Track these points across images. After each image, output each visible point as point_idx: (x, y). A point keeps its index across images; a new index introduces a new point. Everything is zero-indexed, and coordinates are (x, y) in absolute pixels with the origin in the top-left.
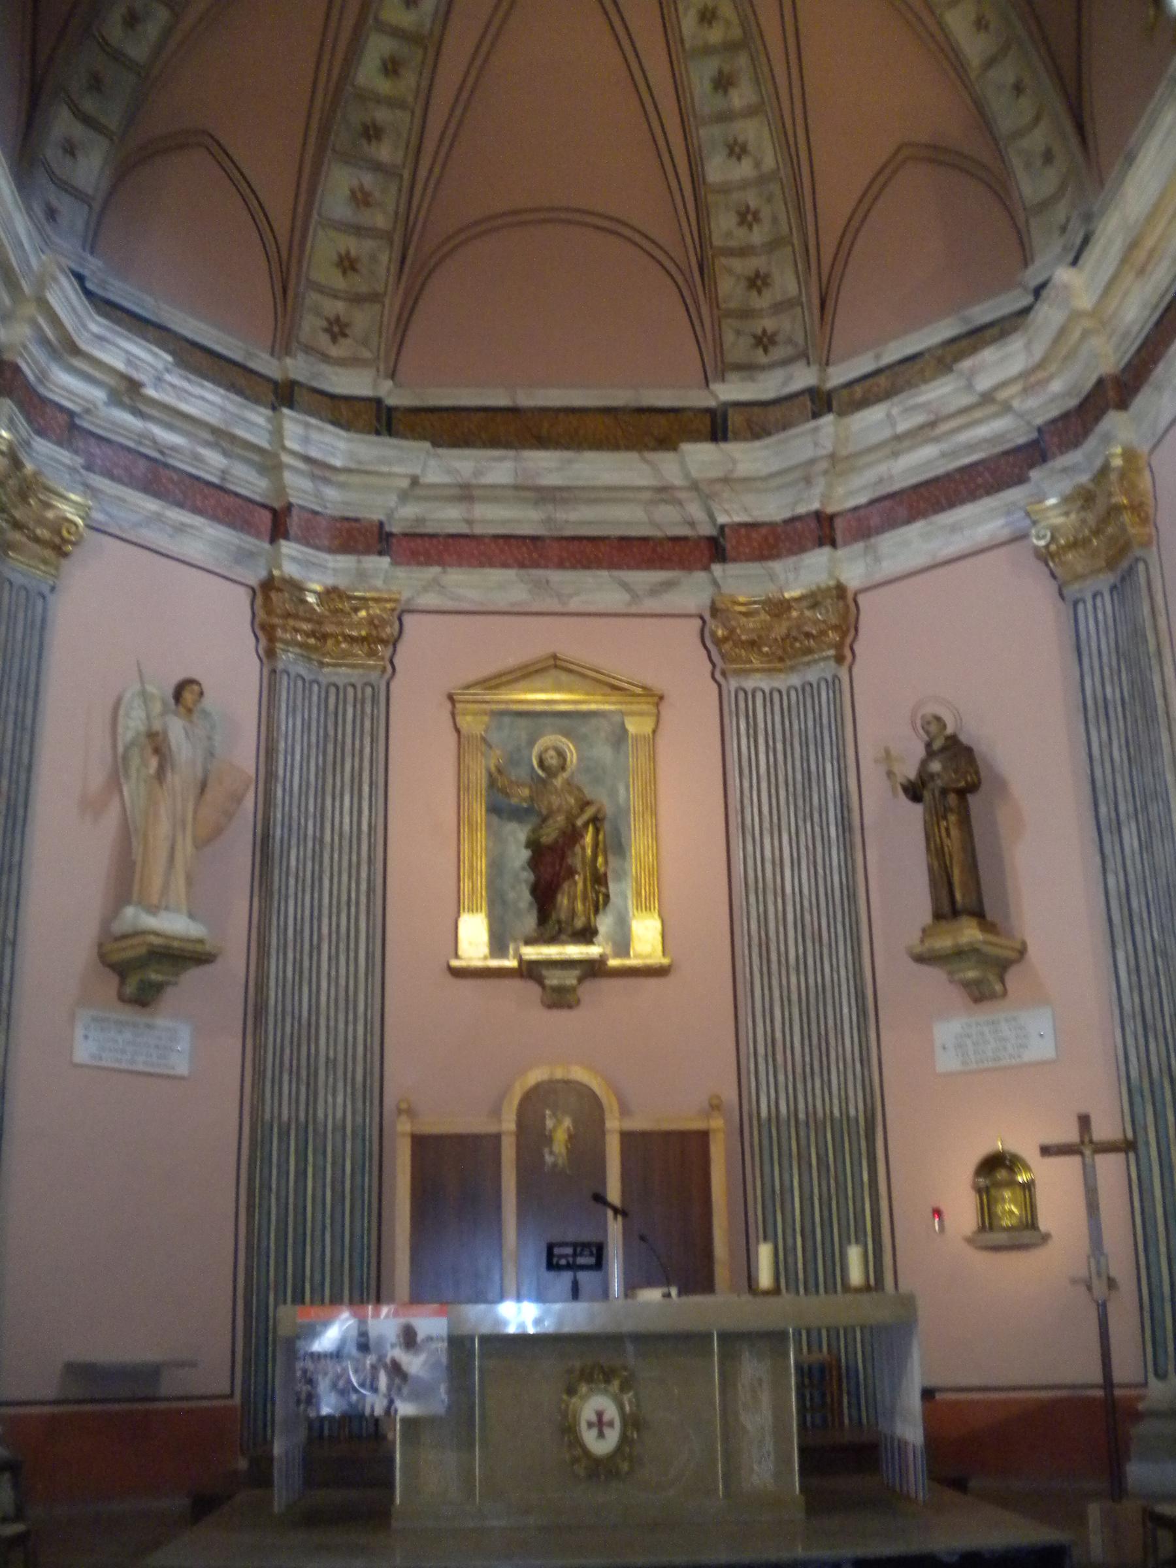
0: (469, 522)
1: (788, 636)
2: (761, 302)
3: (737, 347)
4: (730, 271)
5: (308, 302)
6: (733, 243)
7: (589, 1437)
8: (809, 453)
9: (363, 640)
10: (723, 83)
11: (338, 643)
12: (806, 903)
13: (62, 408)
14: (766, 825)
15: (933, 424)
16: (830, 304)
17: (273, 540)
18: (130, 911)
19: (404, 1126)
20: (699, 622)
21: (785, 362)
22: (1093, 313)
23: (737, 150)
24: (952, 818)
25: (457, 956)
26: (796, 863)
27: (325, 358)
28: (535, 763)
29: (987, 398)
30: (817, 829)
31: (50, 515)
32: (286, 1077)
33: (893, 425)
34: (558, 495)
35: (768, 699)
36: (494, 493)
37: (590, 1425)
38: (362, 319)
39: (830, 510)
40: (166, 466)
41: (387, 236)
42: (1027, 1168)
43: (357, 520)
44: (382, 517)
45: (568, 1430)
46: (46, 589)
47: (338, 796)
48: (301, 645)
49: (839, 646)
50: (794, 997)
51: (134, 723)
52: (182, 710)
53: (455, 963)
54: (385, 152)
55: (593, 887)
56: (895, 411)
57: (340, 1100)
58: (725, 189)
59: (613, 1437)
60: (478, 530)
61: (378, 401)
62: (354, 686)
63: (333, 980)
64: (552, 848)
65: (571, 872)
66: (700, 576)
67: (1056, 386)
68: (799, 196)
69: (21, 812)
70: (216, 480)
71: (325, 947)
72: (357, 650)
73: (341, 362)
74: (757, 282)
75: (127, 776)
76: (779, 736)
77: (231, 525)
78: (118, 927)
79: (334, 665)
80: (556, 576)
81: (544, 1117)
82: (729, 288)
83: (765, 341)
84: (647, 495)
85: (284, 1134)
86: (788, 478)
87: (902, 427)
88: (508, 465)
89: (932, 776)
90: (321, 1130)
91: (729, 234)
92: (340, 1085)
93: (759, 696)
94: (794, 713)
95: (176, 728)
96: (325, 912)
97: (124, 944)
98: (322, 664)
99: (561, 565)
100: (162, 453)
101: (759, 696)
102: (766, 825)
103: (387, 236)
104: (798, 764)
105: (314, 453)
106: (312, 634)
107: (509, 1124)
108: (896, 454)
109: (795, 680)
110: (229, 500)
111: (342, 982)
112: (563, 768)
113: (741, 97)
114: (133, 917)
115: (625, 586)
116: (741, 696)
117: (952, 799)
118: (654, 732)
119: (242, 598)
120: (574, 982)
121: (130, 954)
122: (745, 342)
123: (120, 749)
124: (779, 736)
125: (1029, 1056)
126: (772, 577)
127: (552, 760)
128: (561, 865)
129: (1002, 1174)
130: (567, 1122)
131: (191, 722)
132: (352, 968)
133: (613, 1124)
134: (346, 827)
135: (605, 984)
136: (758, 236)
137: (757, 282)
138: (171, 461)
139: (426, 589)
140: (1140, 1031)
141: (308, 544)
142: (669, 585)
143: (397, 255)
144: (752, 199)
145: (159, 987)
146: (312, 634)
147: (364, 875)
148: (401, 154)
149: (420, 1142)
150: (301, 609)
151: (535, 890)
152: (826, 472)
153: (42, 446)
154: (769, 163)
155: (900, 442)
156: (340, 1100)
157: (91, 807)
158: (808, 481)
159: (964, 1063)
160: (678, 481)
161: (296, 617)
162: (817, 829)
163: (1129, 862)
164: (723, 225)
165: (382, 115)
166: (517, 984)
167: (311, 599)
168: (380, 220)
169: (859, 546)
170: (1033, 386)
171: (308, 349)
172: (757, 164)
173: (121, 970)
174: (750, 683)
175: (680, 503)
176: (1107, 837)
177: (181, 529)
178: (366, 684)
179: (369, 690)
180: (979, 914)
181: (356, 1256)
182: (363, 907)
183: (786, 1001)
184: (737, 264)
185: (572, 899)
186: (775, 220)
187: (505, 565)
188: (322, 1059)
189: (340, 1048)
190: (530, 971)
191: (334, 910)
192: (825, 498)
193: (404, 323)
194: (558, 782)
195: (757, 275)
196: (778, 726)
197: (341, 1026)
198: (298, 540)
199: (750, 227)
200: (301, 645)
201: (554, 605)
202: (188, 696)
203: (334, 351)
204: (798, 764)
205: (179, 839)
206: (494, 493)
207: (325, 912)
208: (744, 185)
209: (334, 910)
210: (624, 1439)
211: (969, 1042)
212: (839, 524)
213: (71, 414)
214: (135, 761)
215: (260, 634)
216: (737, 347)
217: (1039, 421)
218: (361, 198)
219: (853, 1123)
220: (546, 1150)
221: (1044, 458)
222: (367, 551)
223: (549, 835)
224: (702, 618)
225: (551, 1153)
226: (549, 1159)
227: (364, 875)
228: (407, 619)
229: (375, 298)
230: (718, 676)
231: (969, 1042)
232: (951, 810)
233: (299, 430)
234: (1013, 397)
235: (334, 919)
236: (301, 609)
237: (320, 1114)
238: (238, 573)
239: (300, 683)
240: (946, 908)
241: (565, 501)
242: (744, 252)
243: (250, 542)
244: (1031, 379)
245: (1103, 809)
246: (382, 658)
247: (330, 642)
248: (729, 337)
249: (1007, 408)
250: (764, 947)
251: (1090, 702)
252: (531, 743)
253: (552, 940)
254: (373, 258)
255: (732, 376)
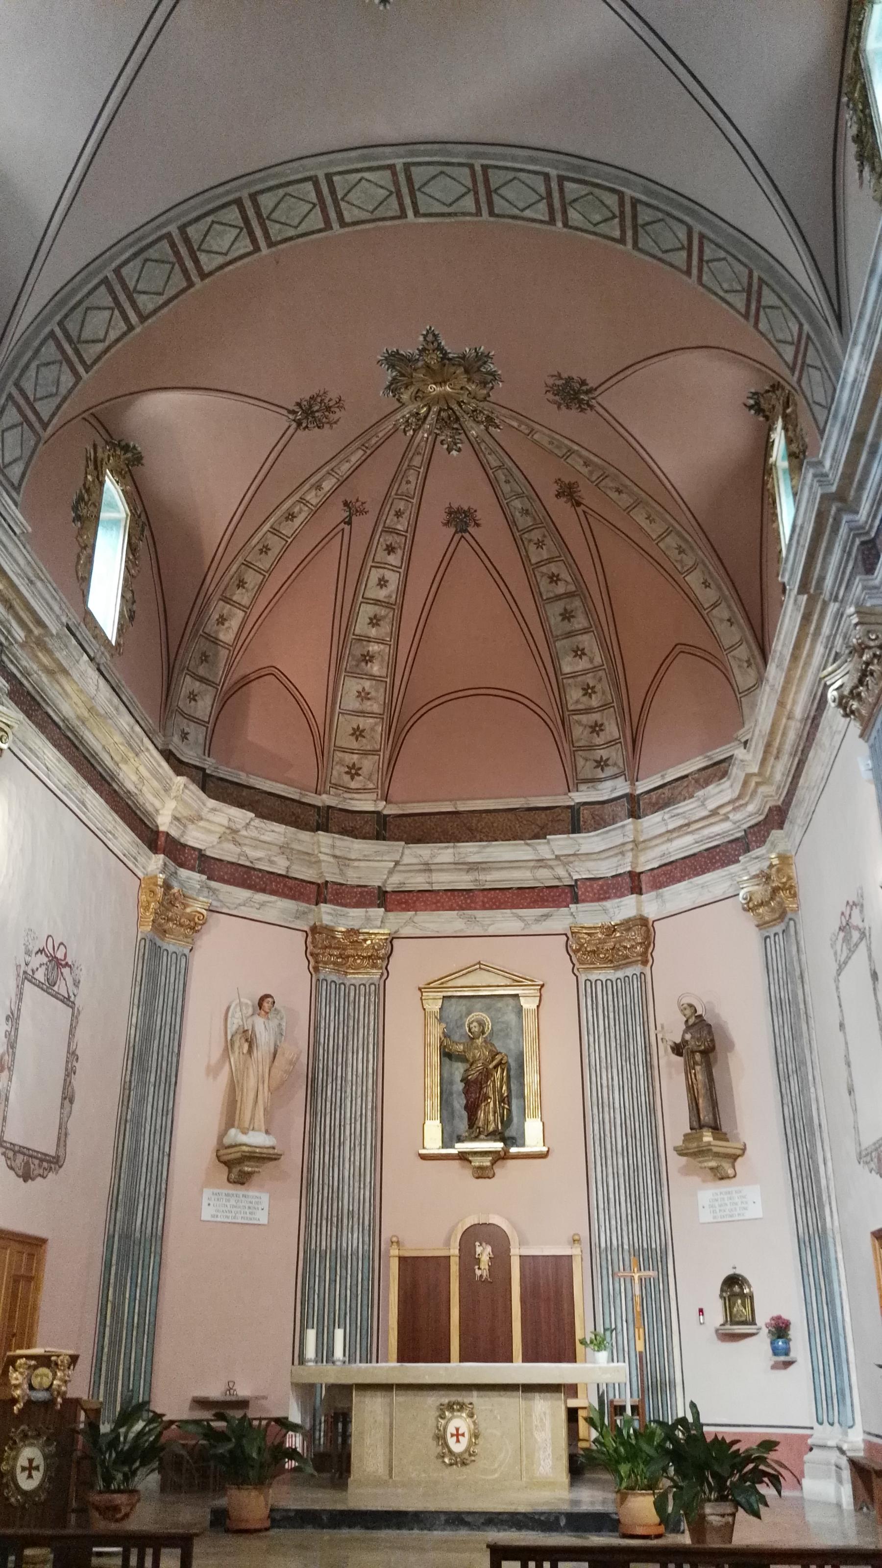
0: (431, 883)
1: (614, 948)
2: (598, 741)
3: (586, 769)
4: (579, 723)
5: (336, 759)
6: (580, 707)
7: (451, 1441)
8: (620, 841)
9: (370, 957)
10: (567, 616)
11: (355, 960)
12: (627, 1114)
13: (194, 849)
14: (604, 1064)
15: (688, 825)
16: (638, 743)
17: (317, 904)
18: (233, 1132)
19: (395, 1252)
20: (565, 938)
21: (615, 777)
22: (760, 774)
23: (579, 653)
24: (698, 1068)
25: (424, 1148)
26: (621, 1088)
27: (348, 790)
28: (467, 1029)
29: (714, 812)
30: (633, 1067)
31: (188, 910)
32: (324, 1222)
33: (666, 825)
34: (480, 866)
35: (604, 985)
36: (443, 868)
37: (452, 1435)
38: (368, 764)
39: (638, 870)
40: (254, 869)
41: (379, 716)
42: (749, 1286)
43: (365, 886)
44: (380, 884)
45: (440, 1438)
46: (186, 951)
47: (355, 1052)
48: (334, 963)
49: (645, 953)
50: (621, 1172)
51: (235, 1023)
52: (263, 1012)
53: (422, 1151)
54: (376, 669)
55: (500, 1104)
56: (666, 817)
57: (355, 1235)
58: (574, 675)
59: (464, 1441)
60: (436, 887)
61: (378, 813)
62: (365, 985)
63: (352, 1162)
64: (476, 1081)
65: (486, 1097)
66: (564, 910)
67: (751, 808)
68: (617, 677)
69: (173, 1080)
70: (284, 873)
71: (348, 1142)
72: (365, 963)
73: (357, 791)
74: (597, 728)
75: (233, 1052)
76: (611, 1009)
77: (293, 898)
78: (227, 1141)
79: (353, 973)
80: (479, 914)
81: (475, 1246)
82: (578, 732)
83: (601, 764)
84: (532, 864)
85: (323, 1258)
86: (611, 853)
87: (671, 827)
88: (451, 851)
89: (687, 1042)
90: (344, 1254)
91: (577, 702)
92: (356, 1227)
93: (599, 983)
94: (620, 995)
95: (259, 1023)
96: (348, 1122)
97: (229, 1151)
98: (346, 973)
99: (484, 908)
100: (252, 862)
101: (599, 983)
102: (604, 1064)
103: (379, 716)
104: (622, 1026)
105: (338, 853)
106: (340, 956)
107: (455, 1251)
108: (670, 840)
109: (620, 974)
110: (290, 883)
111: (357, 1163)
112: (483, 1033)
113: (580, 622)
114: (234, 1135)
115: (520, 918)
116: (588, 983)
117: (698, 1057)
118: (538, 1007)
119: (301, 936)
120: (489, 1164)
121: (233, 1156)
122: (591, 764)
123: (229, 1038)
124: (611, 1009)
125: (748, 1215)
126: (605, 911)
127: (476, 1028)
128: (480, 1093)
129: (736, 1289)
130: (489, 1249)
131: (268, 1019)
132: (363, 1156)
133: (516, 1251)
134: (360, 1071)
135: (510, 1163)
136: (595, 702)
137: (597, 728)
138: (257, 866)
139: (406, 924)
140: (803, 1204)
141: (338, 904)
142: (547, 916)
143: (386, 726)
144: (590, 680)
145: (250, 1174)
146: (340, 956)
147: (370, 1099)
148: (385, 670)
149: (402, 1260)
150: (334, 941)
151: (466, 1108)
152: (632, 850)
153: (184, 873)
154: (598, 660)
155: (670, 834)
156: (355, 1235)
157: (212, 1071)
158: (622, 853)
159: (715, 1217)
160: (549, 856)
161: (330, 947)
162: (633, 1067)
163: (794, 1099)
164: (574, 695)
165: (374, 648)
166: (456, 1164)
167: (339, 936)
168: (376, 708)
169: (653, 893)
170: (738, 807)
171: (336, 786)
172: (591, 660)
173: (229, 1164)
174: (593, 976)
175: (551, 867)
176: (783, 1083)
177: (262, 905)
178: (371, 984)
179: (373, 987)
180: (716, 1128)
181: (364, 1332)
182: (369, 1118)
183: (616, 1175)
184: (584, 718)
185: (486, 1114)
186: (604, 693)
187: (452, 909)
188: (345, 1211)
189: (356, 1205)
190: (463, 1157)
191: (353, 1121)
192: (634, 863)
193: (392, 762)
194: (479, 1041)
195: (596, 724)
196: (611, 1003)
197: (357, 1191)
198: (332, 902)
199: (590, 697)
200: (334, 963)
201: (478, 931)
202: (266, 1005)
203: (353, 785)
204: (622, 1026)
205: (261, 1088)
206: (443, 868)
207: (348, 1122)
208: (585, 672)
209: (353, 1121)
210: (470, 1444)
211: (716, 1204)
212: (643, 877)
213: (200, 850)
214: (237, 1045)
215: (310, 958)
216: (586, 769)
217: (745, 826)
218: (363, 695)
219: (654, 1252)
220: (477, 1267)
221: (747, 850)
222: (371, 905)
223: (473, 1075)
224: (566, 935)
225: (479, 1268)
226: (478, 1272)
227: (370, 1099)
228: (395, 942)
229: (374, 752)
230: (575, 971)
231: (716, 1204)
232: (698, 1064)
233: (330, 842)
234: (729, 812)
235: (353, 1125)
236: (334, 941)
237: (344, 1245)
238: (299, 924)
239: (333, 985)
240: (695, 1124)
241: (484, 869)
242: (588, 711)
243: (303, 906)
244: (736, 803)
245: (781, 1066)
246: (381, 968)
247: (351, 959)
248: (581, 762)
249: (727, 819)
250: (602, 1140)
251: (773, 1000)
252: (469, 1013)
253: (476, 1138)
254: (373, 729)
255: (582, 787)
